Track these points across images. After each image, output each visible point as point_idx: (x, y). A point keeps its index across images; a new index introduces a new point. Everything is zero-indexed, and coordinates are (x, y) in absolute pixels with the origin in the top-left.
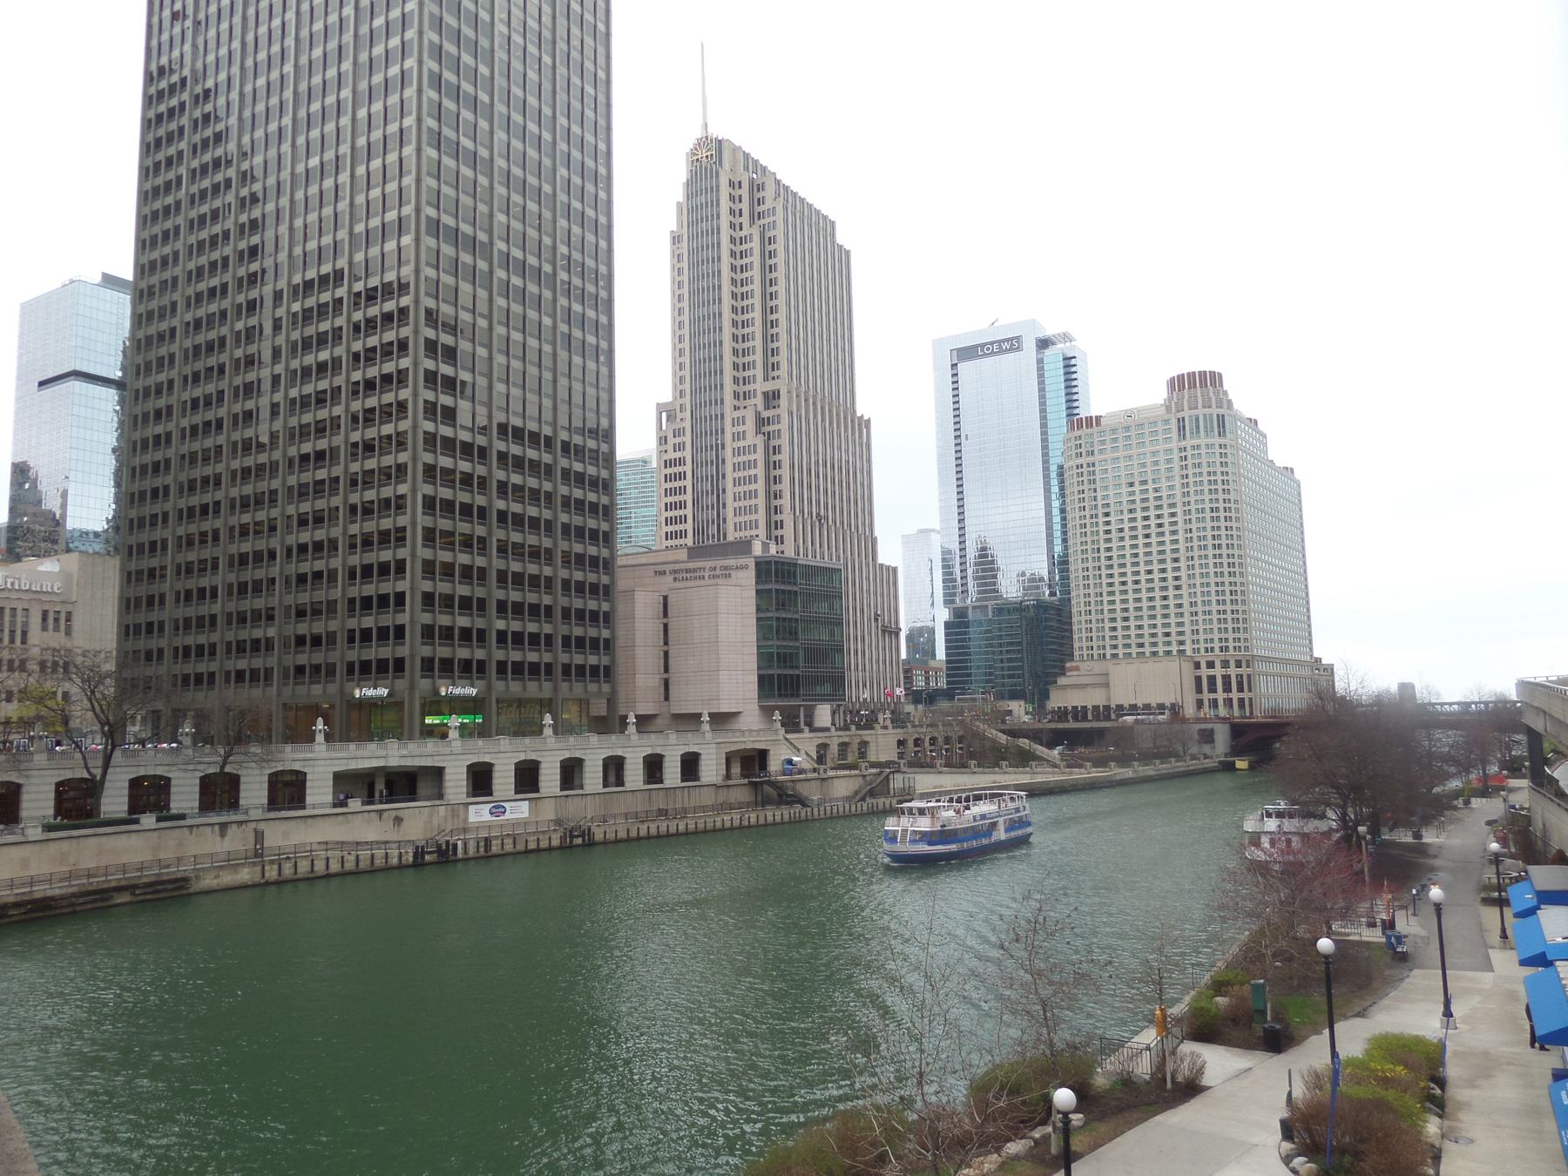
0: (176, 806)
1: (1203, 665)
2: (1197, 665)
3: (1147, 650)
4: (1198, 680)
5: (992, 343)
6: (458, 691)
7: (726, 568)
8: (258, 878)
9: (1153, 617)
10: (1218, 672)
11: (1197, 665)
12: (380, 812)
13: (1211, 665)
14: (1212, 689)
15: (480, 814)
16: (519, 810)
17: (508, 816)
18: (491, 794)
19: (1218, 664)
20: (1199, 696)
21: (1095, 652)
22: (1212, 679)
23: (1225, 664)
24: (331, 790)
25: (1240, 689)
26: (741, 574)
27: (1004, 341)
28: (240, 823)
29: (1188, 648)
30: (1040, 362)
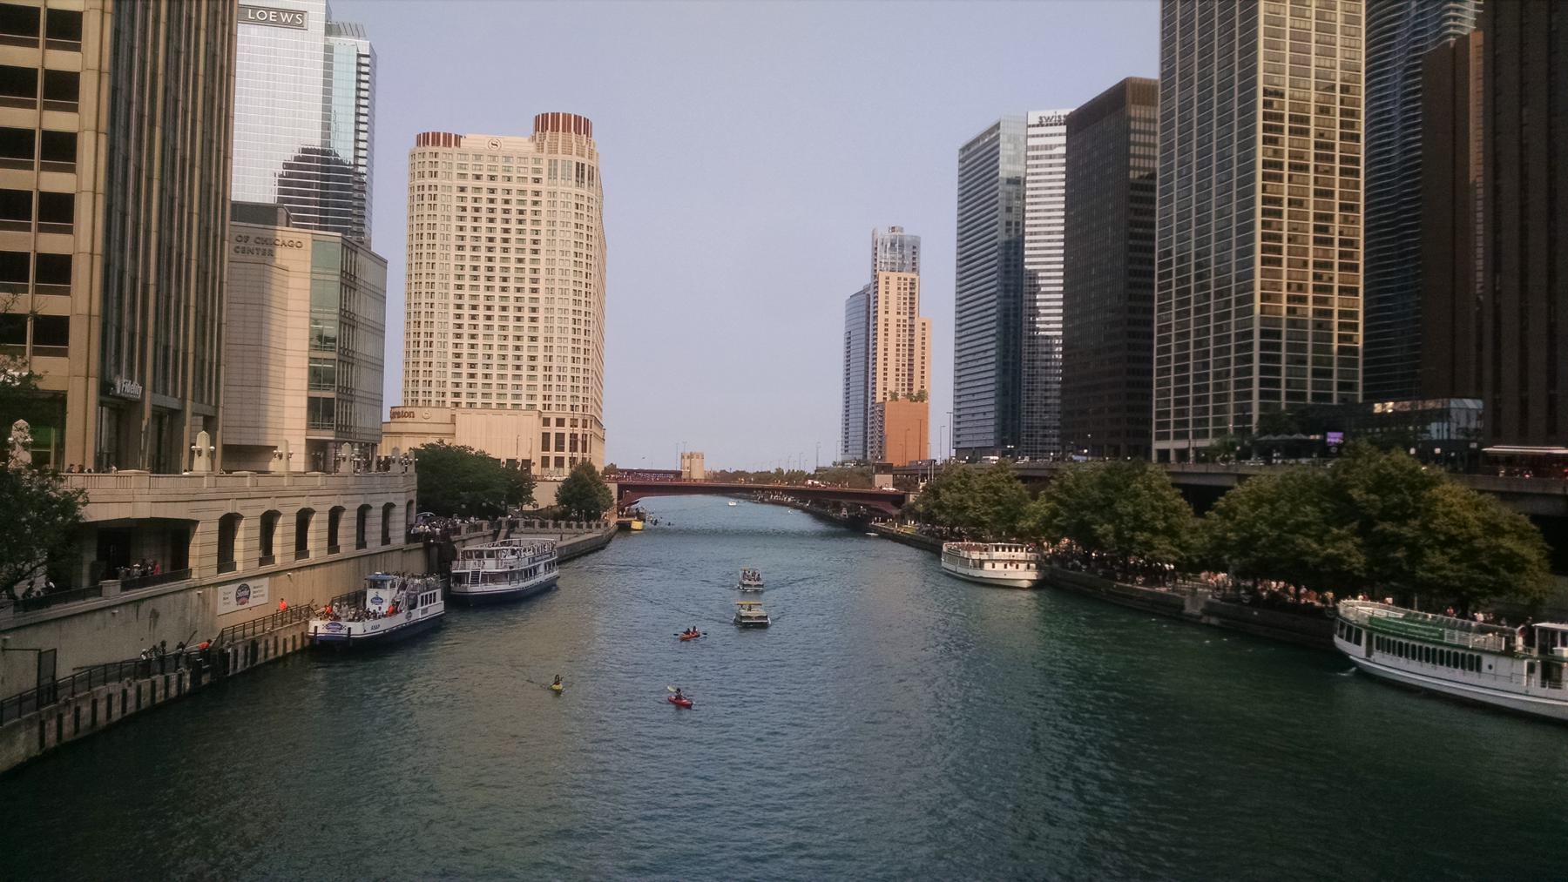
1: (553, 422)
3: (494, 401)
4: (546, 436)
5: (268, 10)
8: (35, 751)
9: (503, 366)
10: (567, 430)
11: (546, 422)
12: (137, 602)
13: (560, 422)
14: (560, 447)
17: (252, 602)
19: (567, 423)
20: (546, 454)
22: (560, 437)
23: (574, 424)
25: (584, 450)
27: (284, 11)
30: (329, 49)
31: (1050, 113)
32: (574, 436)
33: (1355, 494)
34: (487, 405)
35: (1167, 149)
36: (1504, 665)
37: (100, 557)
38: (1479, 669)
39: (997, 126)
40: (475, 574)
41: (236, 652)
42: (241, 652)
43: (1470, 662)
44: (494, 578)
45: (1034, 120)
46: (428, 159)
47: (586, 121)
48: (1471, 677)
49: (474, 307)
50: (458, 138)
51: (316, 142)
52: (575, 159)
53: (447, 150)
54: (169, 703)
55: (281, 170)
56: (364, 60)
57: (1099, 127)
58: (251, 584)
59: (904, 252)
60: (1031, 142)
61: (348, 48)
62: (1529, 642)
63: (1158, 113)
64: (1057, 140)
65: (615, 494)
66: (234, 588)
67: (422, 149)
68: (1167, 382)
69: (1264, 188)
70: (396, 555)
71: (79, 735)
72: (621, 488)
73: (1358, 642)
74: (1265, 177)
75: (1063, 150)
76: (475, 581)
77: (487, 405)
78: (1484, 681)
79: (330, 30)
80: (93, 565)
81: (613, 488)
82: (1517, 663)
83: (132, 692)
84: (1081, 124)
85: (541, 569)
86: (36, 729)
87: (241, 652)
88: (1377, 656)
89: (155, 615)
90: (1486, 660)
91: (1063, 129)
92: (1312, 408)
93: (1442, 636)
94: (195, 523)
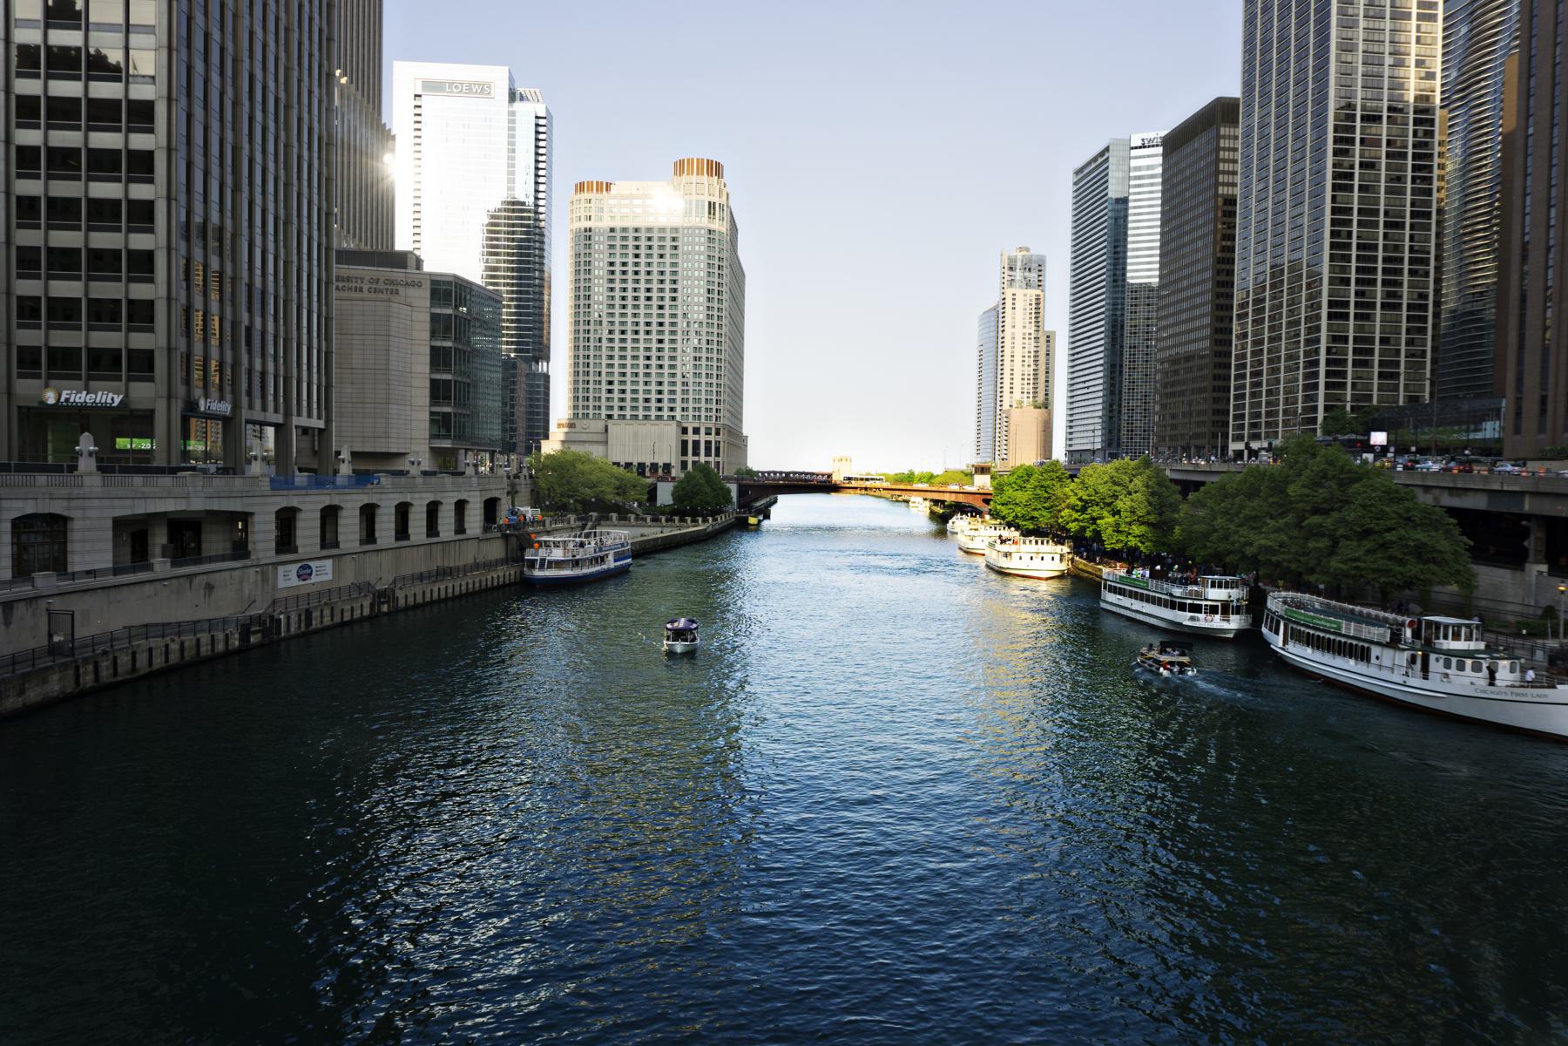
0: (78, 561)
1: (690, 431)
2: (685, 431)
4: (684, 443)
6: (81, 398)
7: (392, 282)
8: (70, 687)
10: (703, 438)
12: (191, 577)
13: (696, 431)
15: (288, 578)
16: (324, 572)
17: (314, 579)
18: (296, 551)
21: (591, 412)
22: (696, 444)
24: (109, 545)
26: (411, 292)
28: (30, 600)
29: (678, 413)
30: (512, 114)
31: (1151, 135)
32: (708, 443)
33: (609, 497)
34: (635, 417)
35: (1247, 157)
36: (1388, 656)
37: (171, 540)
38: (1369, 661)
39: (1107, 149)
40: (543, 560)
41: (288, 619)
42: (294, 618)
43: (1363, 655)
44: (559, 564)
45: (1136, 142)
46: (583, 205)
47: (718, 164)
48: (1361, 667)
49: (623, 332)
50: (608, 186)
51: (524, 192)
52: (707, 199)
53: (599, 196)
54: (214, 658)
55: (487, 220)
56: (542, 122)
57: (1196, 142)
58: (313, 564)
59: (1034, 270)
60: (1134, 163)
61: (526, 112)
62: (1416, 635)
63: (1240, 131)
64: (1153, 161)
65: (734, 494)
66: (294, 568)
67: (579, 196)
68: (1243, 387)
69: (1334, 198)
70: (472, 545)
71: (119, 678)
72: (742, 491)
73: (1277, 633)
74: (1335, 187)
75: (1159, 170)
76: (542, 567)
77: (635, 417)
78: (1372, 671)
79: (513, 97)
80: (164, 546)
81: (733, 488)
82: (1398, 653)
83: (174, 647)
84: (1174, 143)
85: (611, 558)
86: (71, 672)
87: (294, 618)
88: (1291, 647)
89: (209, 587)
90: (1375, 651)
91: (1160, 150)
92: (1376, 409)
93: (1339, 628)
94: (252, 514)
